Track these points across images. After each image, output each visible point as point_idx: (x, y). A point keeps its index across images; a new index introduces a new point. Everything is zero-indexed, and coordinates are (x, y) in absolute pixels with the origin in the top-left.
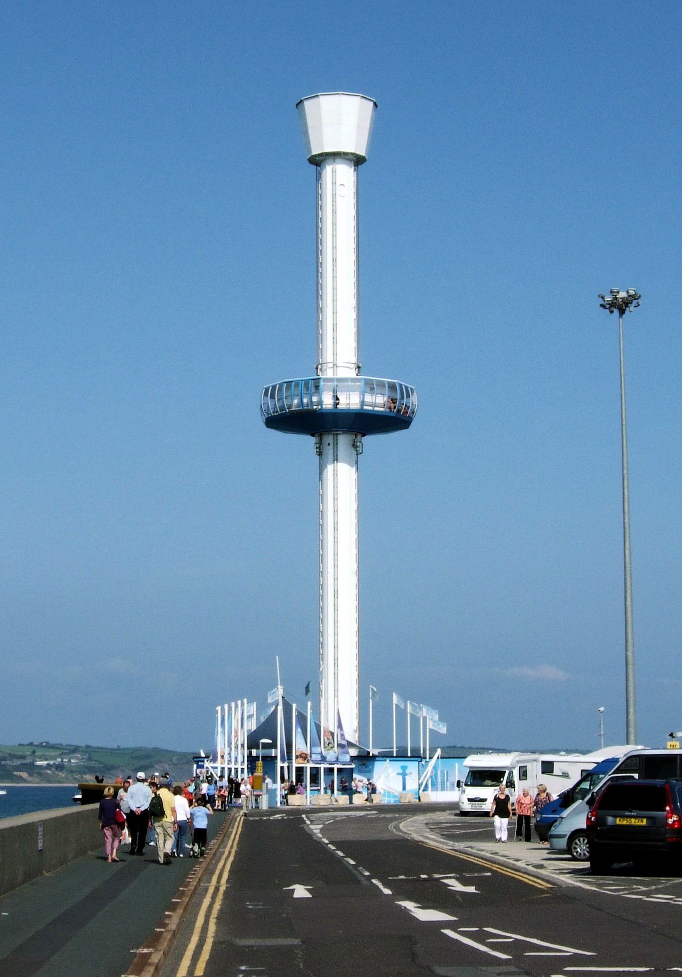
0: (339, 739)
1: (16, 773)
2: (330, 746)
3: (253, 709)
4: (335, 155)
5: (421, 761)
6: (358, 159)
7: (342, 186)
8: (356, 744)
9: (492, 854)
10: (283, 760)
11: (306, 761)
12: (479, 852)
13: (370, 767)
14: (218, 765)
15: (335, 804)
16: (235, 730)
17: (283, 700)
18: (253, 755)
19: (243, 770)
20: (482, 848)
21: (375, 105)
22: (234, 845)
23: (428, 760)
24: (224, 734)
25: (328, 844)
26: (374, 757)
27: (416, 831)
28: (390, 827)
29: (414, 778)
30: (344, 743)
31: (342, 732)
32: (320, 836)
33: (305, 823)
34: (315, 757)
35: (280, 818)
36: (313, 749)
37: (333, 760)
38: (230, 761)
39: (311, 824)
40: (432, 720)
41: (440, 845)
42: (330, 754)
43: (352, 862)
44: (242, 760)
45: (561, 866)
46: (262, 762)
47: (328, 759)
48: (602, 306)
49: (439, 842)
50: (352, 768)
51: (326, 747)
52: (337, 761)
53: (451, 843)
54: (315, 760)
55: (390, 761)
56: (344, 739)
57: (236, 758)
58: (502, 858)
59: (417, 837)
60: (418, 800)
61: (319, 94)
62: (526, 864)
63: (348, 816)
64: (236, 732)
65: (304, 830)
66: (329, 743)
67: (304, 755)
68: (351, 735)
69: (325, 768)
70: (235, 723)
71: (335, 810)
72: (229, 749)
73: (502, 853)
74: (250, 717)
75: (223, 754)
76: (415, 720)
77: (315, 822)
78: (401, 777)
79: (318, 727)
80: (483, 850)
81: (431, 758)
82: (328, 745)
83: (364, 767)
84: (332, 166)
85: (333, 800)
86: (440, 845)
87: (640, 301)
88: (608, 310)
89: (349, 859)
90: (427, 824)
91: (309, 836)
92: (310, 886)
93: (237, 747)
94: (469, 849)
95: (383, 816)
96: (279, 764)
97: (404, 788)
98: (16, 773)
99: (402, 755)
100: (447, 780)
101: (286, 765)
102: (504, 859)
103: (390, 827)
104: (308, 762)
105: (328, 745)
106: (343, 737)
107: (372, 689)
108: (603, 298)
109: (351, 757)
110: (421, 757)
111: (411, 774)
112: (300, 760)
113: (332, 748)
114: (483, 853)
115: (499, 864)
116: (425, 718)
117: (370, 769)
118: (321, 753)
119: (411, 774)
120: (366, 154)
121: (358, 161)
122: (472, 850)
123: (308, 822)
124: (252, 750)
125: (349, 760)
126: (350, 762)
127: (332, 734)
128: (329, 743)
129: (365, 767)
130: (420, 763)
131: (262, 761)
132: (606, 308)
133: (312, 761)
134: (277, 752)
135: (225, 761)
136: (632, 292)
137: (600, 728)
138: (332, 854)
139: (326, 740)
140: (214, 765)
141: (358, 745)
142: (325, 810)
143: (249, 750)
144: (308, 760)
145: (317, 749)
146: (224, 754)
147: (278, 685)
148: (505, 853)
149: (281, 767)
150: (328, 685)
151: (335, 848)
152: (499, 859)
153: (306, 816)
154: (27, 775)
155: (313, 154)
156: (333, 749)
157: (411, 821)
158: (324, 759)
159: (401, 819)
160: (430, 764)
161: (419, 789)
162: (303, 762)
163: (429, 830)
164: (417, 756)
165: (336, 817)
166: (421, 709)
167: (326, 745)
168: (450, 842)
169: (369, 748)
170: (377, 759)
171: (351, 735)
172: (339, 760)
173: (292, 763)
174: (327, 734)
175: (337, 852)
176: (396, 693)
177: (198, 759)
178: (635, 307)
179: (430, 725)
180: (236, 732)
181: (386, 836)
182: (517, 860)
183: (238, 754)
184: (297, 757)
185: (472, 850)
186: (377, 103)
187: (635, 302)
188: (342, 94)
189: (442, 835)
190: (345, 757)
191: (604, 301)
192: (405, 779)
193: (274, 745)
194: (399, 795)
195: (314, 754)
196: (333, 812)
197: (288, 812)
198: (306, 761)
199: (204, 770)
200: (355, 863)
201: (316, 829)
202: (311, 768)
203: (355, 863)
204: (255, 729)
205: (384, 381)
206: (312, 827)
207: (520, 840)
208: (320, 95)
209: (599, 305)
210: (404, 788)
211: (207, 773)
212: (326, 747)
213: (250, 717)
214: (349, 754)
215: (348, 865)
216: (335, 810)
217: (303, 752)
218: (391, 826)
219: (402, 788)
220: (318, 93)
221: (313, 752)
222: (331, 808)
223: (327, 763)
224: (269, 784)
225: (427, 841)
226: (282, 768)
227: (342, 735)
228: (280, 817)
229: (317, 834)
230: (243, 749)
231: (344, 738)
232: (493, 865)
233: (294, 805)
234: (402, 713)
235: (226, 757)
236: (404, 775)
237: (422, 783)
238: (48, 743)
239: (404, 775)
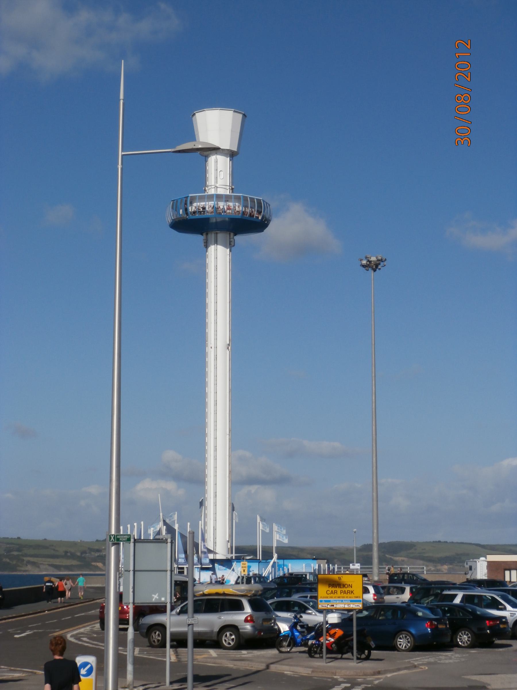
1: (93, 564)
6: (233, 153)
7: (220, 172)
21: (244, 115)
22: (82, 626)
30: (206, 550)
34: (181, 560)
54: (181, 562)
55: (237, 562)
84: (215, 156)
87: (385, 263)
98: (93, 564)
121: (232, 154)
126: (209, 563)
136: (380, 258)
147: (160, 513)
154: (102, 565)
176: (276, 523)
178: (382, 267)
186: (245, 114)
187: (382, 264)
190: (206, 560)
195: (181, 558)
207: (471, 568)
214: (208, 558)
224: (210, 573)
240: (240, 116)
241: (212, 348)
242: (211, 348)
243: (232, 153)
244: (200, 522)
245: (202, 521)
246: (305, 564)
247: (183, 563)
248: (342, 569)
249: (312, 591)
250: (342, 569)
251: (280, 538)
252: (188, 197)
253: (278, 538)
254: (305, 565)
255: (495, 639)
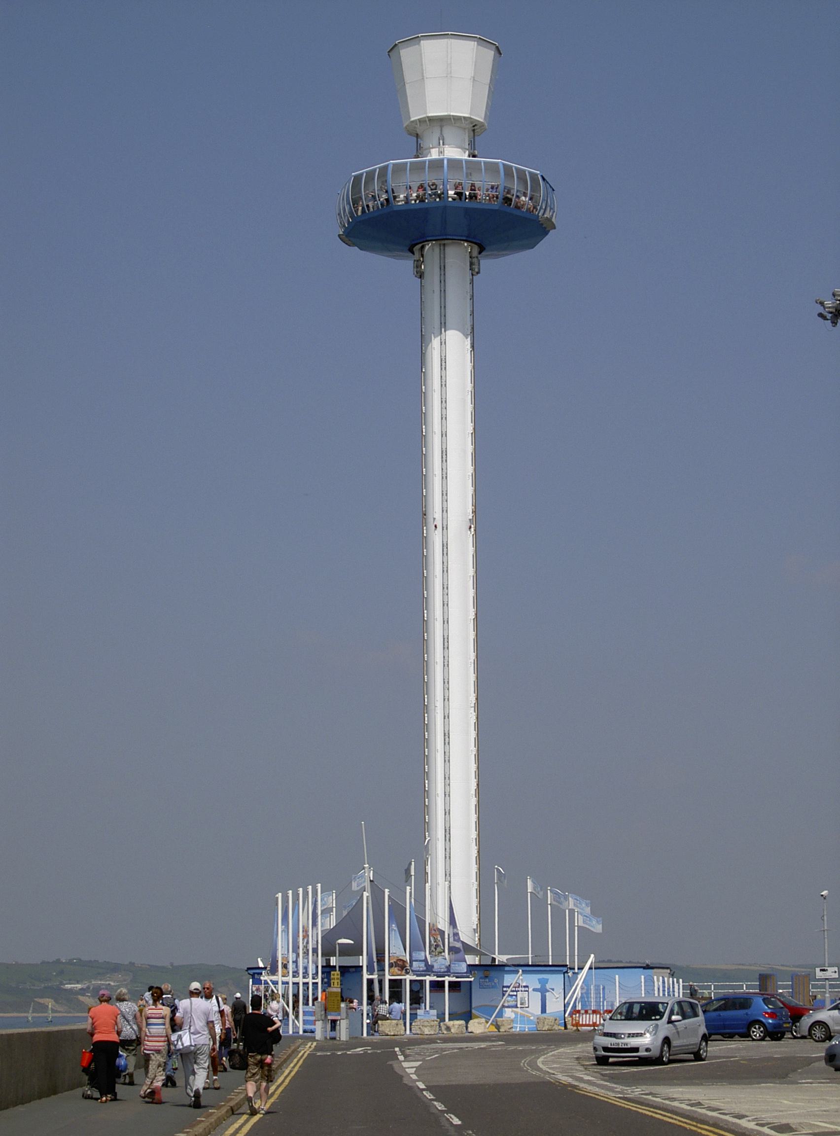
0: (451, 940)
2: (438, 949)
3: (332, 900)
4: (442, 121)
5: (567, 972)
6: (475, 128)
8: (476, 947)
9: (692, 1105)
10: (370, 970)
11: (404, 971)
12: (667, 1102)
13: (496, 981)
14: (279, 978)
15: (445, 1032)
16: (303, 927)
17: (371, 885)
18: (332, 964)
19: (315, 984)
20: (671, 1096)
21: (498, 50)
23: (576, 970)
24: (288, 932)
25: (424, 1090)
26: (502, 966)
27: (563, 1071)
28: (522, 1064)
29: (557, 996)
30: (458, 945)
31: (455, 930)
32: (414, 1077)
33: (398, 1059)
35: (361, 1052)
36: (414, 954)
37: (442, 970)
38: (296, 974)
39: (404, 1061)
40: (581, 914)
41: (602, 1092)
42: (438, 961)
43: (456, 1121)
44: (314, 972)
45: (818, 1126)
46: (339, 973)
47: (436, 968)
48: (821, 315)
49: (599, 1086)
50: (471, 982)
51: (433, 951)
52: (448, 971)
53: (619, 1088)
56: (459, 940)
57: (306, 968)
58: (710, 1113)
59: (564, 1079)
60: (563, 1028)
61: (420, 35)
62: (757, 1124)
63: (461, 1048)
64: (306, 931)
65: (393, 1068)
66: (437, 946)
67: (400, 963)
68: (467, 932)
69: (431, 982)
70: (304, 919)
71: (445, 1040)
72: (295, 955)
73: (707, 1103)
74: (327, 911)
75: (285, 962)
76: (558, 914)
77: (411, 1058)
78: (539, 994)
79: (421, 923)
80: (674, 1099)
81: (581, 969)
82: (436, 949)
83: (487, 980)
85: (443, 1028)
86: (602, 1092)
88: (830, 321)
89: (452, 1116)
90: (578, 1059)
91: (398, 1078)
92: (575, 1092)
93: (306, 953)
94: (650, 1097)
95: (513, 1048)
96: (366, 976)
97: (544, 1010)
99: (538, 967)
100: (604, 999)
101: (375, 977)
102: (714, 1114)
103: (522, 1064)
104: (407, 973)
105: (436, 949)
106: (456, 938)
107: (498, 869)
108: (822, 304)
109: (469, 966)
110: (566, 966)
111: (553, 989)
112: (395, 970)
113: (441, 953)
114: (676, 1104)
115: (709, 1125)
116: (572, 912)
117: (495, 983)
118: (426, 960)
119: (553, 989)
120: (485, 119)
122: (654, 1099)
123: (401, 1058)
124: (332, 958)
125: (465, 971)
127: (442, 933)
128: (437, 946)
129: (489, 981)
130: (566, 975)
131: (339, 971)
132: (828, 319)
133: (412, 971)
134: (363, 961)
135: (288, 973)
137: (823, 920)
138: (426, 1106)
139: (433, 942)
140: (274, 978)
141: (479, 949)
142: (431, 1040)
143: (324, 958)
144: (406, 970)
145: (419, 954)
146: (288, 962)
148: (714, 1104)
149: (368, 980)
150: (437, 865)
151: (432, 1097)
152: (706, 1115)
153: (400, 1050)
155: (412, 119)
156: (443, 954)
157: (552, 1055)
158: (429, 969)
159: (540, 1053)
160: (579, 976)
161: (565, 1012)
162: (399, 972)
163: (582, 1068)
164: (561, 968)
165: (443, 1050)
166: (566, 898)
167: (433, 949)
168: (618, 1086)
169: (495, 954)
170: (507, 968)
171: (467, 932)
172: (451, 971)
173: (384, 975)
174: (433, 932)
175: (435, 1103)
177: (255, 973)
179: (579, 921)
180: (306, 931)
181: (516, 1078)
182: (741, 1117)
183: (308, 962)
184: (391, 965)
185: (654, 1099)
186: (499, 47)
188: (451, 34)
189: (602, 1075)
191: (825, 308)
192: (545, 996)
193: (356, 950)
194: (536, 1020)
195: (416, 961)
196: (441, 1043)
197: (374, 1045)
198: (404, 971)
199: (262, 987)
200: (460, 1123)
201: (409, 1068)
202: (411, 981)
203: (460, 1123)
204: (334, 925)
205: (497, 164)
206: (405, 1064)
208: (422, 36)
209: (816, 315)
210: (544, 1010)
211: (267, 991)
212: (433, 951)
213: (327, 911)
214: (466, 962)
215: (447, 1125)
216: (445, 1040)
217: (400, 958)
218: (524, 1063)
219: (540, 1009)
220: (419, 34)
221: (413, 959)
222: (440, 1039)
223: (434, 975)
225: (582, 1085)
226: (370, 982)
227: (456, 935)
228: (362, 1050)
229: (411, 1075)
230: (315, 954)
231: (459, 938)
232: (699, 1125)
233: (388, 1035)
234: (539, 904)
235: (291, 967)
236: (543, 991)
237: (569, 1004)
238: (80, 960)
239: (543, 991)
240: (490, 54)
241: (437, 526)
242: (436, 526)
243: (474, 126)
244: (408, 888)
245: (411, 886)
246: (644, 975)
247: (422, 971)
248: (713, 989)
249: (408, 1039)
250: (713, 989)
251: (584, 922)
252: (418, 191)
253: (581, 924)
254: (645, 978)
255: (106, 1096)
